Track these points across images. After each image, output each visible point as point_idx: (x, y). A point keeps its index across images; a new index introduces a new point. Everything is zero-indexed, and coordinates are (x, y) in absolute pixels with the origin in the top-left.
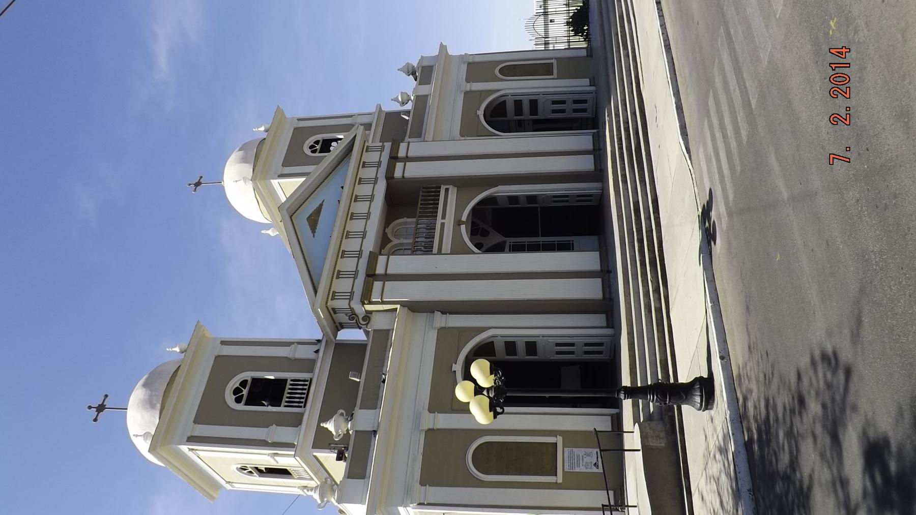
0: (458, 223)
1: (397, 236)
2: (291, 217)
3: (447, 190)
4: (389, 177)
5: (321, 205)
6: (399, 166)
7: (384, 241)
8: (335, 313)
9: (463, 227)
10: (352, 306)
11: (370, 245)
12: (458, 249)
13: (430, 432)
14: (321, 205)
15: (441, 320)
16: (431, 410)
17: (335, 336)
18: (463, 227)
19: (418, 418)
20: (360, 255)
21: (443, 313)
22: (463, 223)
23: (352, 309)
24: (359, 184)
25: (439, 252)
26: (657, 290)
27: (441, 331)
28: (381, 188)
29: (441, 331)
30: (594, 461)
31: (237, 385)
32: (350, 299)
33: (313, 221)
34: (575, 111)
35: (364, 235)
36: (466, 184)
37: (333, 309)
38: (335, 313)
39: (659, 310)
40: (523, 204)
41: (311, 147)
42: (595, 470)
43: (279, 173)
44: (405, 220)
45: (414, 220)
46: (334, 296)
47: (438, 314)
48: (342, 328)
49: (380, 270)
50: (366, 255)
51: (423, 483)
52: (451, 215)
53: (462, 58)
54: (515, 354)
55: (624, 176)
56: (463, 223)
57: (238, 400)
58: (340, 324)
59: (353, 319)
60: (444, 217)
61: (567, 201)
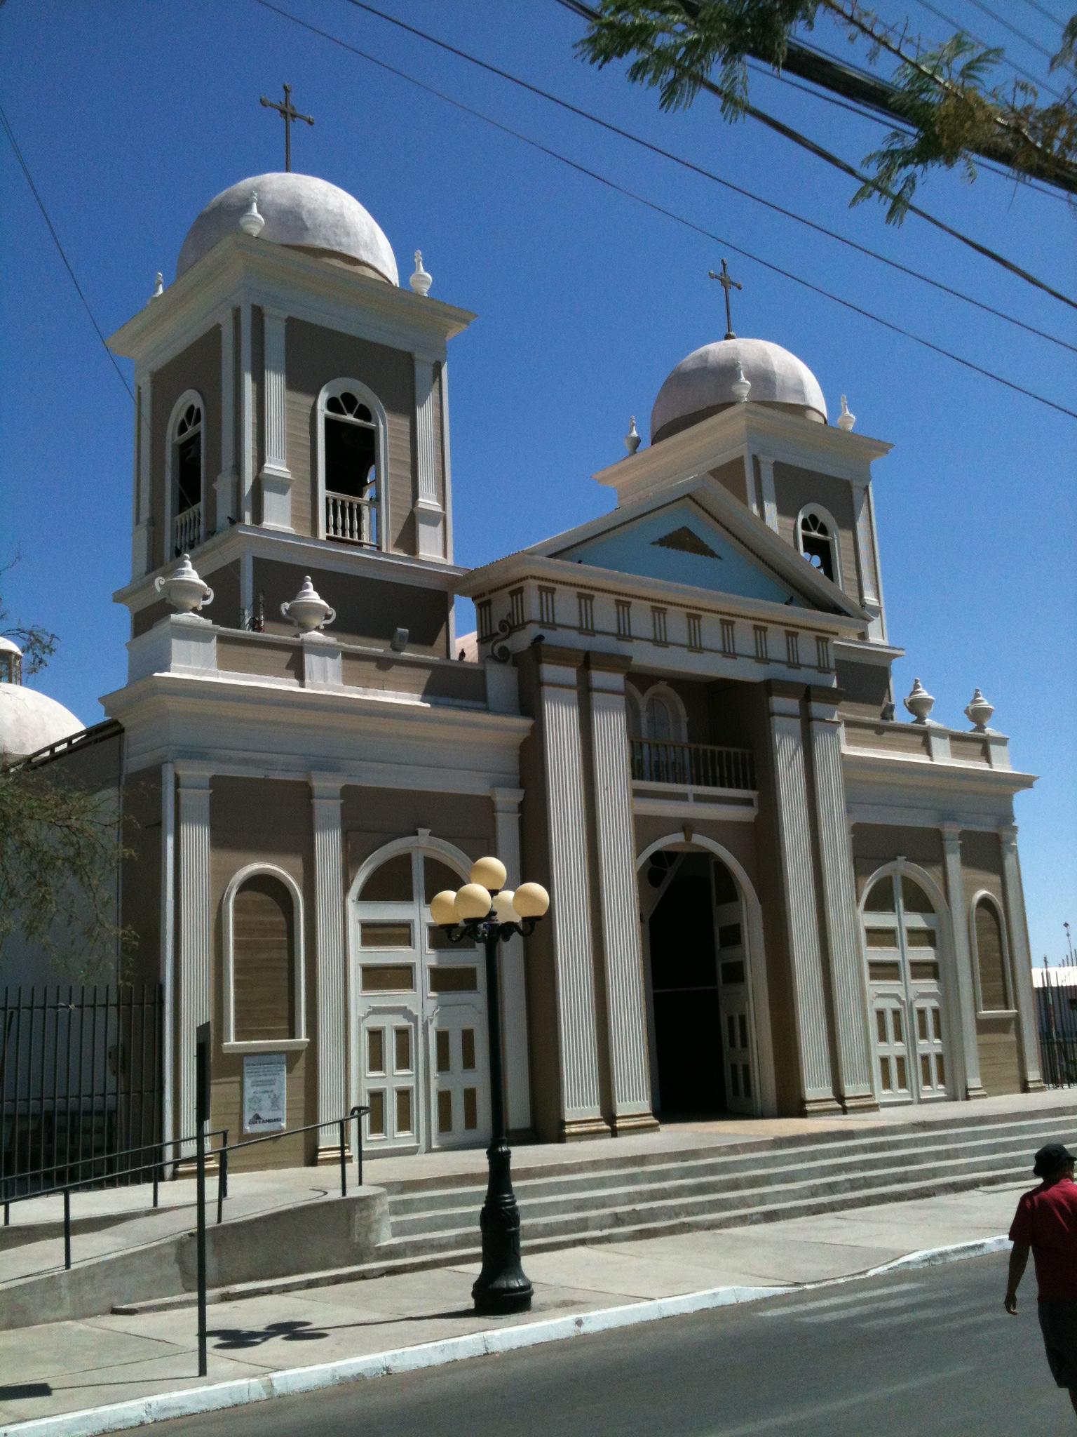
0: (687, 827)
1: (652, 702)
2: (689, 496)
3: (748, 802)
4: (770, 687)
5: (711, 554)
6: (792, 705)
7: (641, 680)
8: (512, 593)
9: (679, 838)
10: (528, 627)
11: (645, 656)
12: (644, 828)
13: (305, 793)
14: (711, 554)
15: (507, 799)
16: (348, 793)
17: (463, 594)
18: (679, 838)
19: (329, 766)
20: (624, 635)
21: (522, 806)
22: (688, 838)
23: (523, 626)
24: (756, 628)
25: (637, 793)
26: (618, 1220)
27: (488, 804)
28: (746, 671)
29: (488, 804)
30: (264, 1115)
31: (361, 401)
32: (542, 624)
33: (682, 540)
34: (469, 1062)
35: (660, 642)
36: (762, 841)
37: (521, 590)
38: (512, 593)
39: (583, 1225)
40: (724, 956)
41: (813, 518)
42: (248, 1117)
43: (761, 458)
44: (684, 719)
45: (685, 740)
46: (547, 591)
47: (516, 796)
48: (480, 607)
49: (599, 678)
50: (627, 648)
51: (216, 782)
52: (707, 810)
53: (1006, 819)
54: (726, 981)
55: (814, 1156)
56: (688, 838)
57: (332, 404)
58: (488, 603)
59: (503, 628)
60: (699, 798)
61: (732, 1044)
